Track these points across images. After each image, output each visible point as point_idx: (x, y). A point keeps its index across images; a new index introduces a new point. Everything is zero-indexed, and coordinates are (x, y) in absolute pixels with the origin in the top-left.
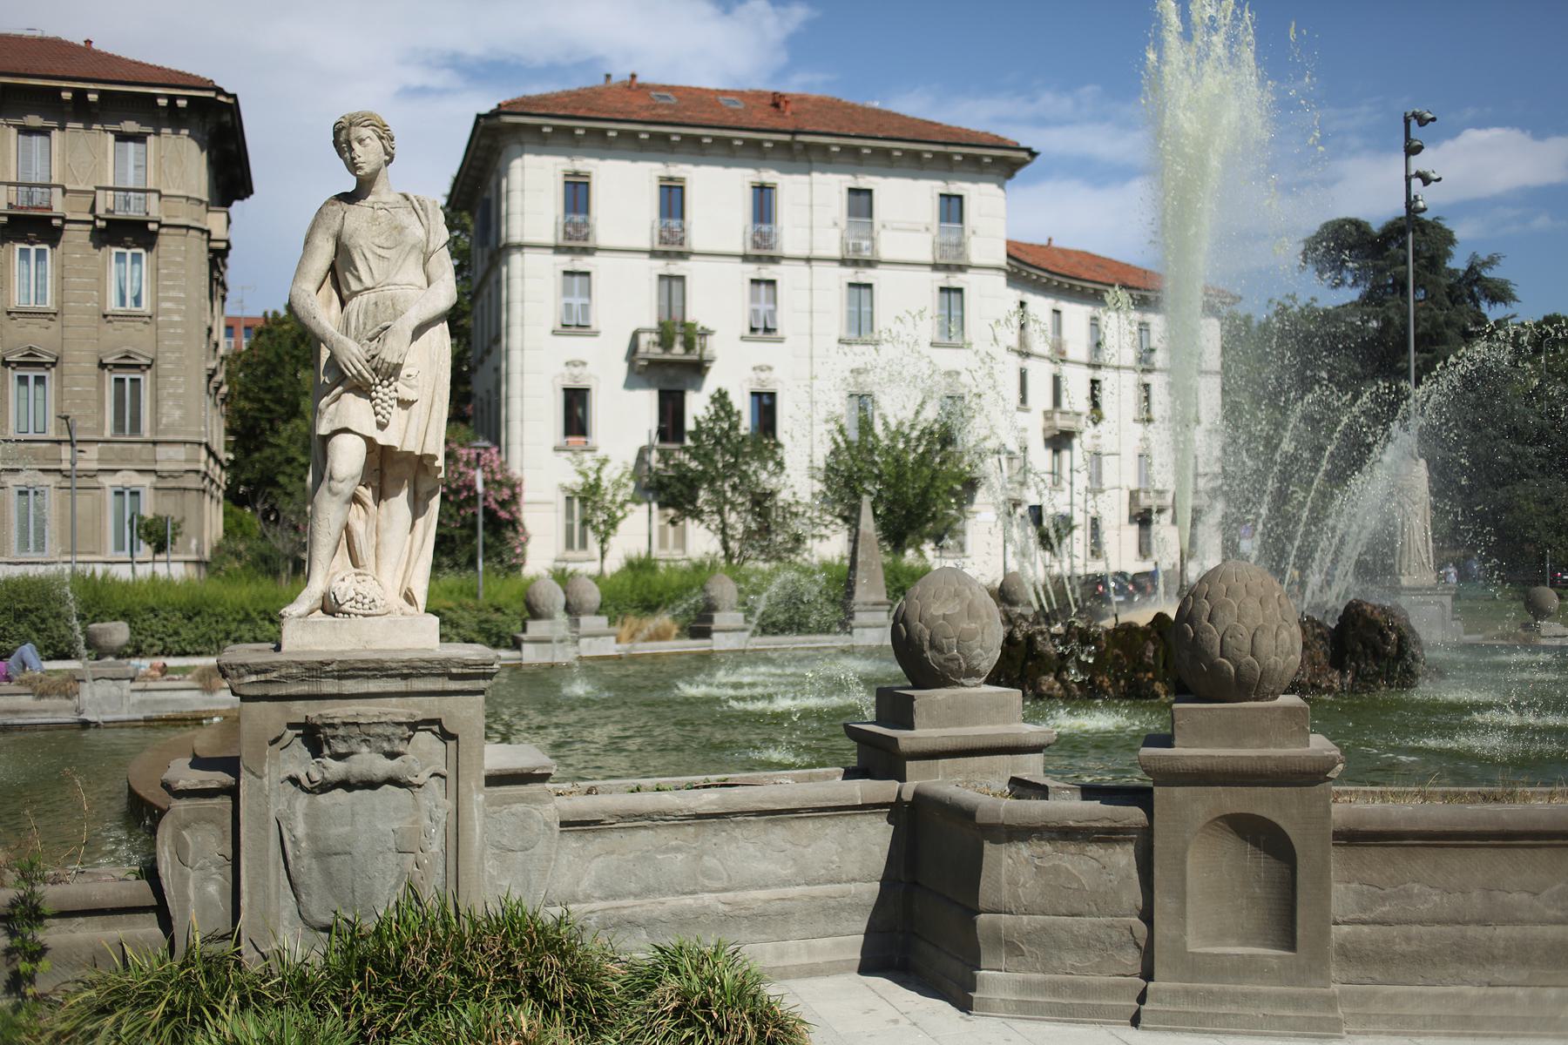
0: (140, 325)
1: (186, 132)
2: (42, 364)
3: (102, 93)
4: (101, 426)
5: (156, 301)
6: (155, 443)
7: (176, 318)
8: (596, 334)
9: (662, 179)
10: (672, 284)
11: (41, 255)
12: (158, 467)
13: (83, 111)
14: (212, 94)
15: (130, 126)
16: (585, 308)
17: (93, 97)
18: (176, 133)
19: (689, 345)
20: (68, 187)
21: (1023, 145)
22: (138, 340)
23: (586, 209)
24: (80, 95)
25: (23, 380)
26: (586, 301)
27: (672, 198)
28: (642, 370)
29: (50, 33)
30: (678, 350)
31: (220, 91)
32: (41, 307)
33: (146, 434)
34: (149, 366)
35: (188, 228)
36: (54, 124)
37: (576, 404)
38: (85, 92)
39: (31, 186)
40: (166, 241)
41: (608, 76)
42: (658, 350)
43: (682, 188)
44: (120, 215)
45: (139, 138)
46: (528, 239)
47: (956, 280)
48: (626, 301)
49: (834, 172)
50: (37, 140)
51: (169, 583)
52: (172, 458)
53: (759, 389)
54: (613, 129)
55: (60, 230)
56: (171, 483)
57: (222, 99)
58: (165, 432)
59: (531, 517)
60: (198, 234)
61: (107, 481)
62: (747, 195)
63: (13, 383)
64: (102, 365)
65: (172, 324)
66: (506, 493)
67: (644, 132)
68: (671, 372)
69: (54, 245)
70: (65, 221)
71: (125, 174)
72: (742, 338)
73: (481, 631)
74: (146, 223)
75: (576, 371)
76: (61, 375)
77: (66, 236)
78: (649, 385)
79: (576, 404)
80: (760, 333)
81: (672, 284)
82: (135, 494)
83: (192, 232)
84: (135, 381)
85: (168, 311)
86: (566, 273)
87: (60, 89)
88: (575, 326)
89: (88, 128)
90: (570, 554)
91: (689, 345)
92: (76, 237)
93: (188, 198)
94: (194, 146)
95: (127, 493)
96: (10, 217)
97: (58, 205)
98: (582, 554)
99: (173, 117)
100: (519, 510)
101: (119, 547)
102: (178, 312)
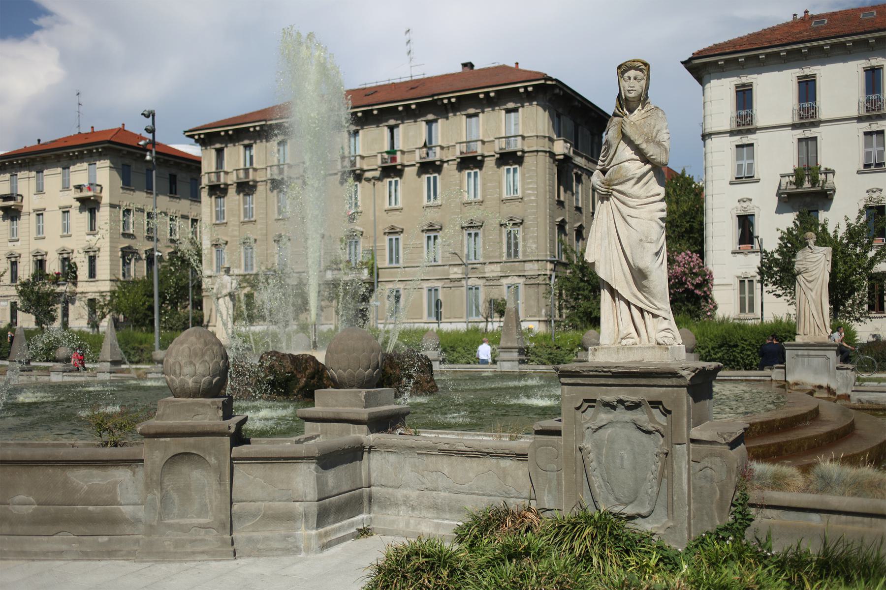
0: (517, 203)
1: (535, 103)
2: (435, 230)
3: (457, 97)
4: (501, 256)
5: (523, 192)
6: (524, 261)
7: (533, 198)
8: (758, 181)
9: (737, 87)
10: (808, 145)
11: (515, 170)
12: (526, 274)
13: (490, 102)
14: (543, 82)
15: (511, 105)
16: (750, 166)
17: (492, 94)
18: (531, 104)
19: (814, 181)
20: (525, 135)
21: (554, 77)
22: (515, 210)
23: (750, 106)
24: (487, 94)
25: (470, 234)
26: (750, 161)
27: (807, 89)
28: (787, 200)
29: (501, 64)
30: (807, 185)
31: (550, 79)
32: (397, 207)
33: (521, 258)
34: (521, 223)
35: (537, 151)
36: (479, 111)
37: (746, 223)
38: (489, 92)
39: (508, 137)
40: (528, 160)
41: (39, 141)
42: (794, 187)
43: (815, 80)
44: (507, 150)
45: (515, 110)
46: (714, 129)
47: (746, 140)
48: (777, 157)
49: (725, 77)
50: (474, 119)
51: (457, 332)
52: (531, 269)
53: (742, 213)
54: (762, 54)
55: (522, 157)
56: (532, 281)
57: (549, 82)
58: (528, 256)
59: (717, 294)
60: (543, 154)
61: (504, 281)
62: (862, 75)
63: (466, 237)
64: (463, 228)
65: (531, 201)
66: (699, 280)
67: (762, 54)
68: (808, 199)
69: (439, 174)
70: (523, 152)
71: (510, 130)
72: (859, 172)
73: (549, 359)
74: (515, 152)
75: (745, 205)
76: (524, 228)
77: (486, 164)
78: (792, 210)
79: (746, 223)
80: (873, 167)
81: (808, 145)
82: (436, 290)
83: (540, 153)
84: (397, 239)
85: (529, 195)
86: (737, 146)
87: (478, 94)
88: (744, 177)
89: (493, 110)
90: (743, 316)
91: (814, 181)
92: (490, 163)
93: (537, 136)
94: (540, 109)
95: (746, 281)
96: (461, 158)
97: (479, 149)
98: (751, 316)
99: (528, 97)
100: (710, 290)
101: (430, 315)
102: (533, 195)
